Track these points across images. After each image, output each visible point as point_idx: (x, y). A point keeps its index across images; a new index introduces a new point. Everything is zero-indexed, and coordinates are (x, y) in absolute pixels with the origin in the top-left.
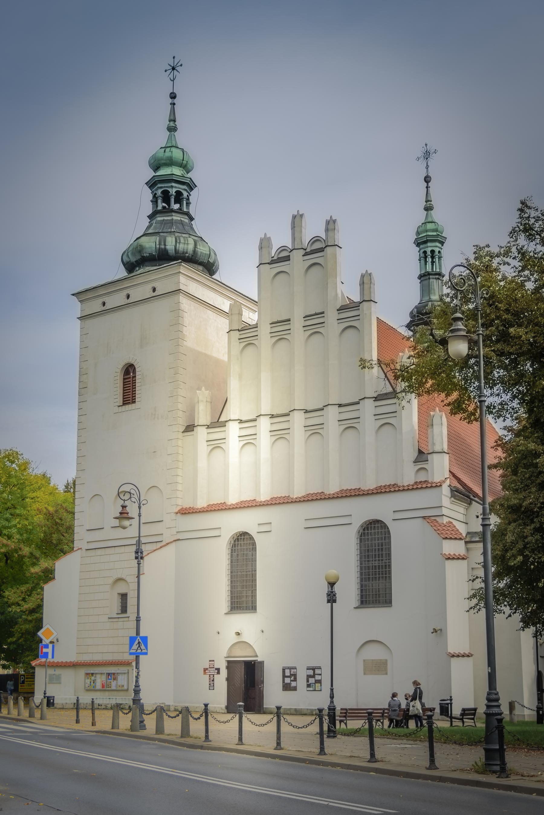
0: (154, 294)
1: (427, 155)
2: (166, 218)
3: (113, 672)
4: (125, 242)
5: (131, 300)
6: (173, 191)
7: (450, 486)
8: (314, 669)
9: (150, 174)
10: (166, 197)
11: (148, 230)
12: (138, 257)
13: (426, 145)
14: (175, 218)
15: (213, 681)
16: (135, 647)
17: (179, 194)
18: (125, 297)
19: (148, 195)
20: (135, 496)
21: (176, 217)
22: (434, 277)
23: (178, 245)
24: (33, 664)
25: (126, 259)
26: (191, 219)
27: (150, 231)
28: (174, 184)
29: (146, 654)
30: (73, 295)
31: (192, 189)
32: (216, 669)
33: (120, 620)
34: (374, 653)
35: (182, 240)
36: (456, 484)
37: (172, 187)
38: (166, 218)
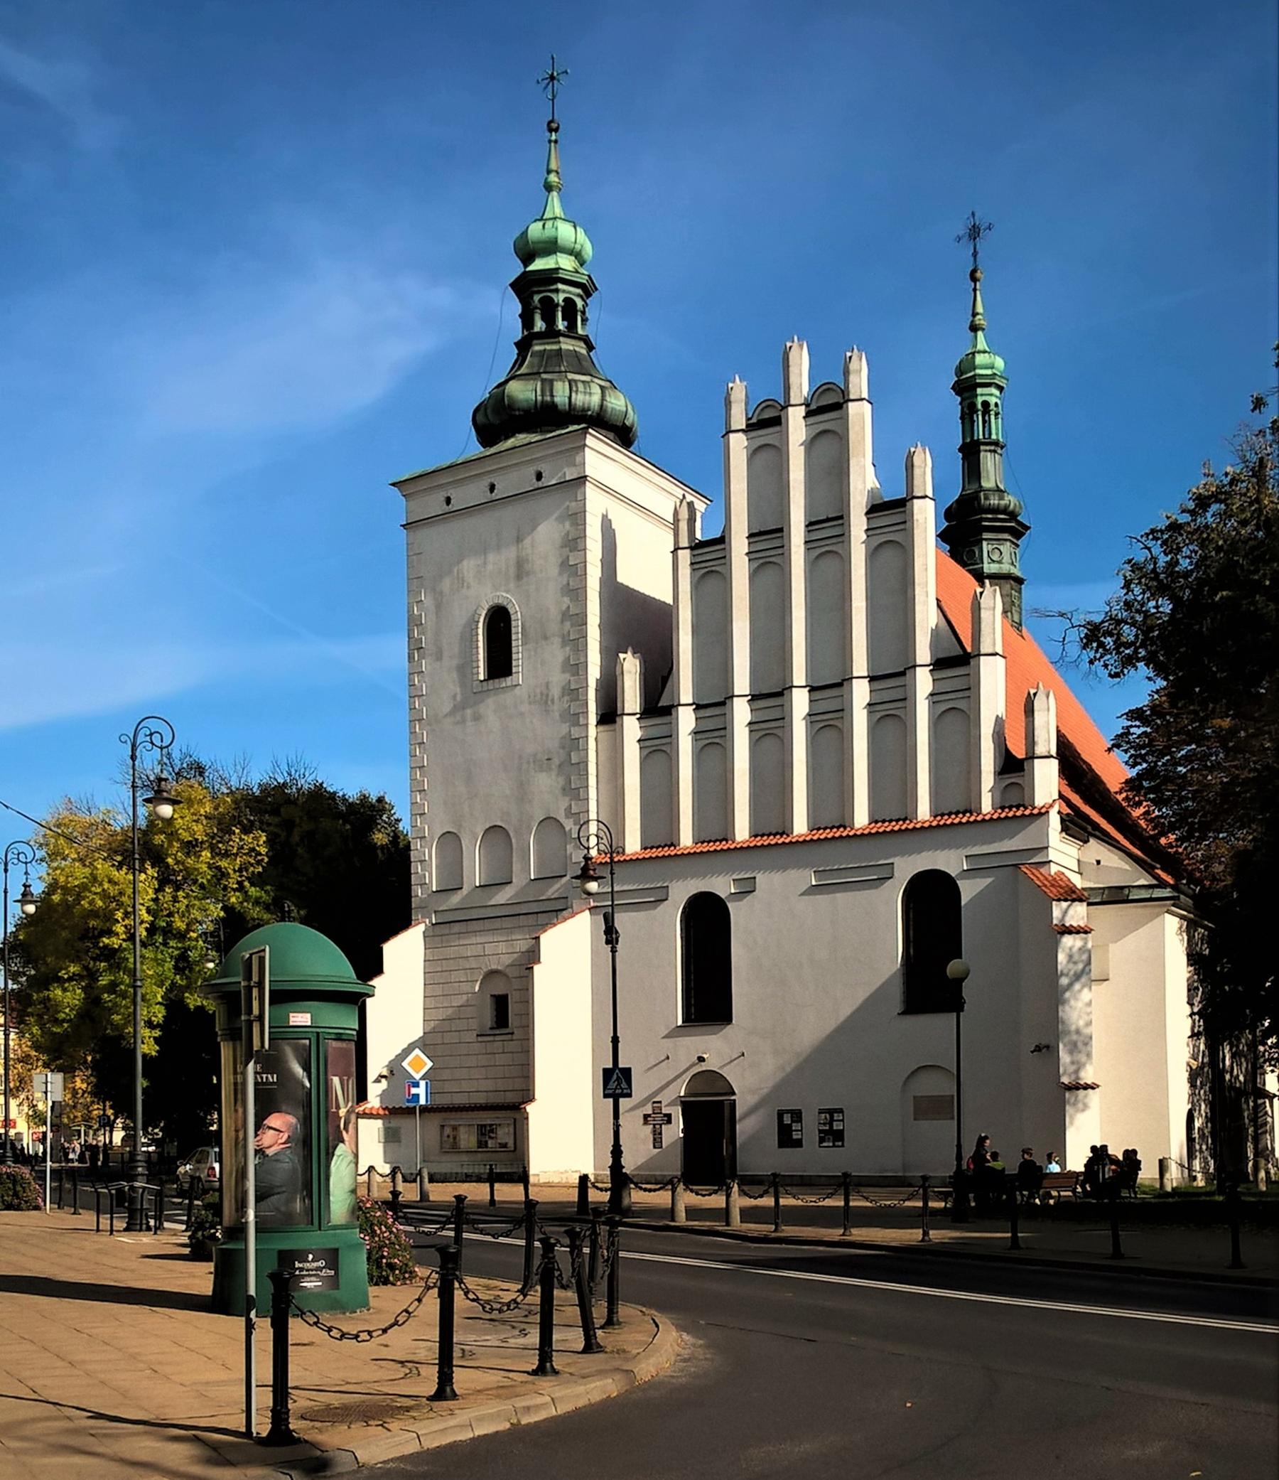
0: (540, 484)
1: (974, 233)
2: (548, 347)
4: (480, 392)
5: (498, 494)
7: (1059, 812)
8: (831, 1112)
9: (517, 269)
10: (548, 309)
11: (519, 369)
13: (973, 214)
14: (564, 347)
16: (612, 1085)
17: (569, 302)
18: (487, 489)
19: (515, 306)
20: (605, 841)
21: (567, 345)
22: (988, 448)
23: (574, 395)
26: (590, 347)
27: (523, 370)
28: (560, 286)
29: (630, 1095)
30: (393, 485)
31: (588, 295)
32: (666, 1115)
33: (497, 1038)
36: (1067, 810)
37: (557, 291)
38: (548, 347)
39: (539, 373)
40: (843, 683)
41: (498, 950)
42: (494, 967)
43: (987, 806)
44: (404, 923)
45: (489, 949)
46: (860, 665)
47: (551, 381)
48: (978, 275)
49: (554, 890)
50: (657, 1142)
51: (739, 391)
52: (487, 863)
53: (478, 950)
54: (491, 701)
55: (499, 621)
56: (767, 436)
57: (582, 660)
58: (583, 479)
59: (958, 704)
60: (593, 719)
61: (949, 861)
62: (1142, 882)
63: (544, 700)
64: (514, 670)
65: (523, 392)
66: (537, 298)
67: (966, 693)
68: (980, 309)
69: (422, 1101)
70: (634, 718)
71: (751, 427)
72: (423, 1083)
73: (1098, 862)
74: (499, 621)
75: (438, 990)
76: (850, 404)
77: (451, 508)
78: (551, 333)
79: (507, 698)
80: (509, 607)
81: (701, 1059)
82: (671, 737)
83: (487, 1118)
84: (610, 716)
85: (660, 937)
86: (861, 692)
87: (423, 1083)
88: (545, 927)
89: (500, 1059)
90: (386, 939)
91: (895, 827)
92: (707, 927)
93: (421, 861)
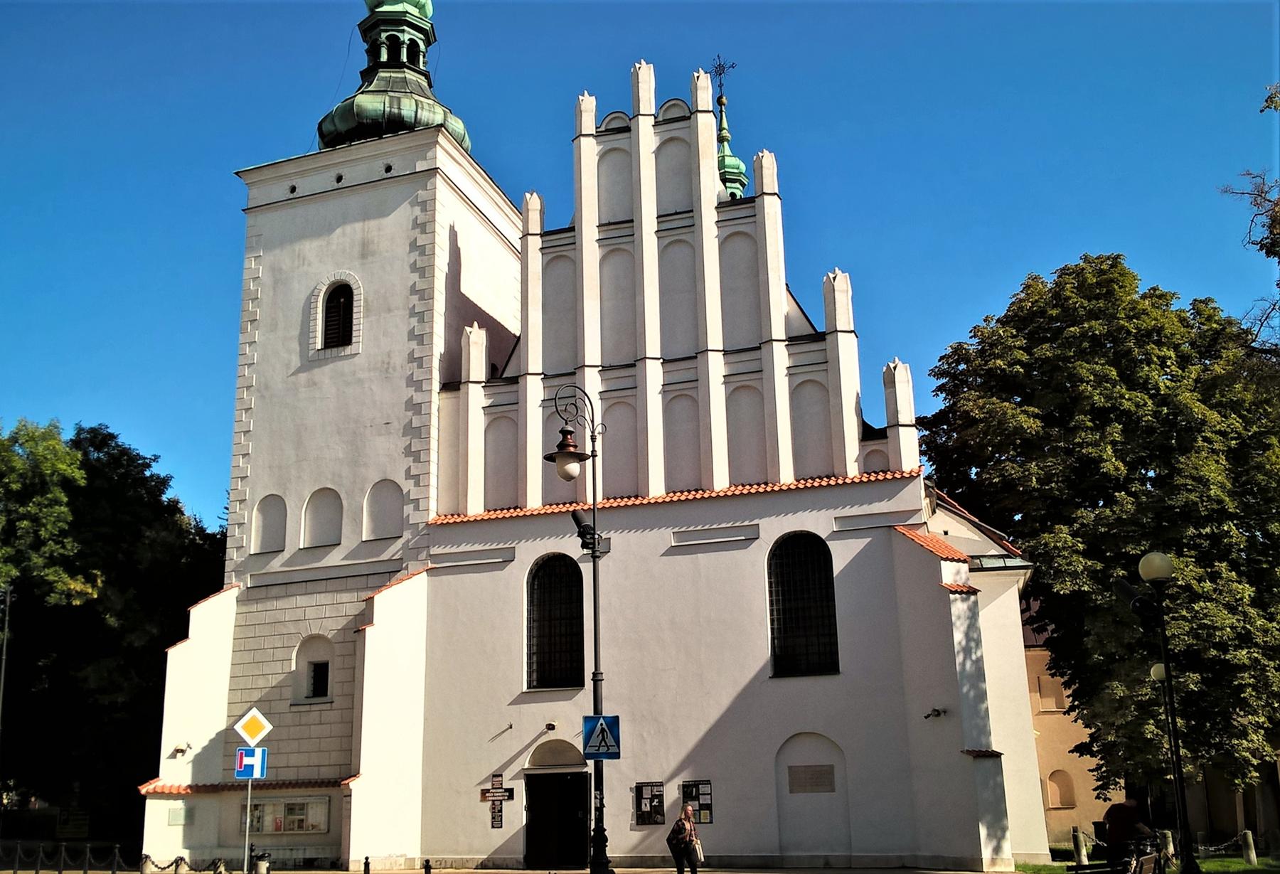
0: (389, 175)
3: (299, 800)
6: (405, 38)
10: (395, 44)
12: (353, 124)
15: (501, 811)
16: (595, 740)
17: (413, 44)
18: (334, 179)
21: (410, 75)
24: (144, 790)
25: (328, 127)
29: (616, 756)
32: (506, 790)
33: (314, 708)
34: (807, 755)
35: (426, 106)
37: (403, 31)
39: (386, 91)
40: (699, 353)
41: (324, 614)
42: (315, 631)
43: (853, 471)
44: (216, 586)
45: (311, 613)
46: (715, 338)
47: (399, 99)
48: (724, 100)
49: (393, 551)
50: (497, 821)
51: (588, 104)
52: (316, 526)
53: (299, 614)
54: (328, 369)
55: (340, 301)
56: (619, 141)
57: (428, 330)
58: (434, 171)
59: (816, 378)
60: (436, 386)
61: (818, 522)
62: (993, 552)
63: (385, 369)
64: (354, 340)
65: (371, 103)
66: (384, 35)
67: (823, 367)
68: (725, 125)
69: (257, 774)
70: (480, 386)
71: (598, 135)
72: (258, 752)
73: (946, 533)
74: (340, 301)
75: (248, 657)
76: (699, 115)
77: (295, 195)
78: (394, 63)
79: (344, 365)
80: (352, 283)
81: (551, 727)
82: (517, 404)
83: (296, 796)
84: (453, 383)
85: (504, 604)
86: (717, 367)
87: (258, 752)
88: (379, 588)
89: (316, 731)
90: (195, 600)
91: (757, 492)
92: (556, 590)
93: (240, 525)
